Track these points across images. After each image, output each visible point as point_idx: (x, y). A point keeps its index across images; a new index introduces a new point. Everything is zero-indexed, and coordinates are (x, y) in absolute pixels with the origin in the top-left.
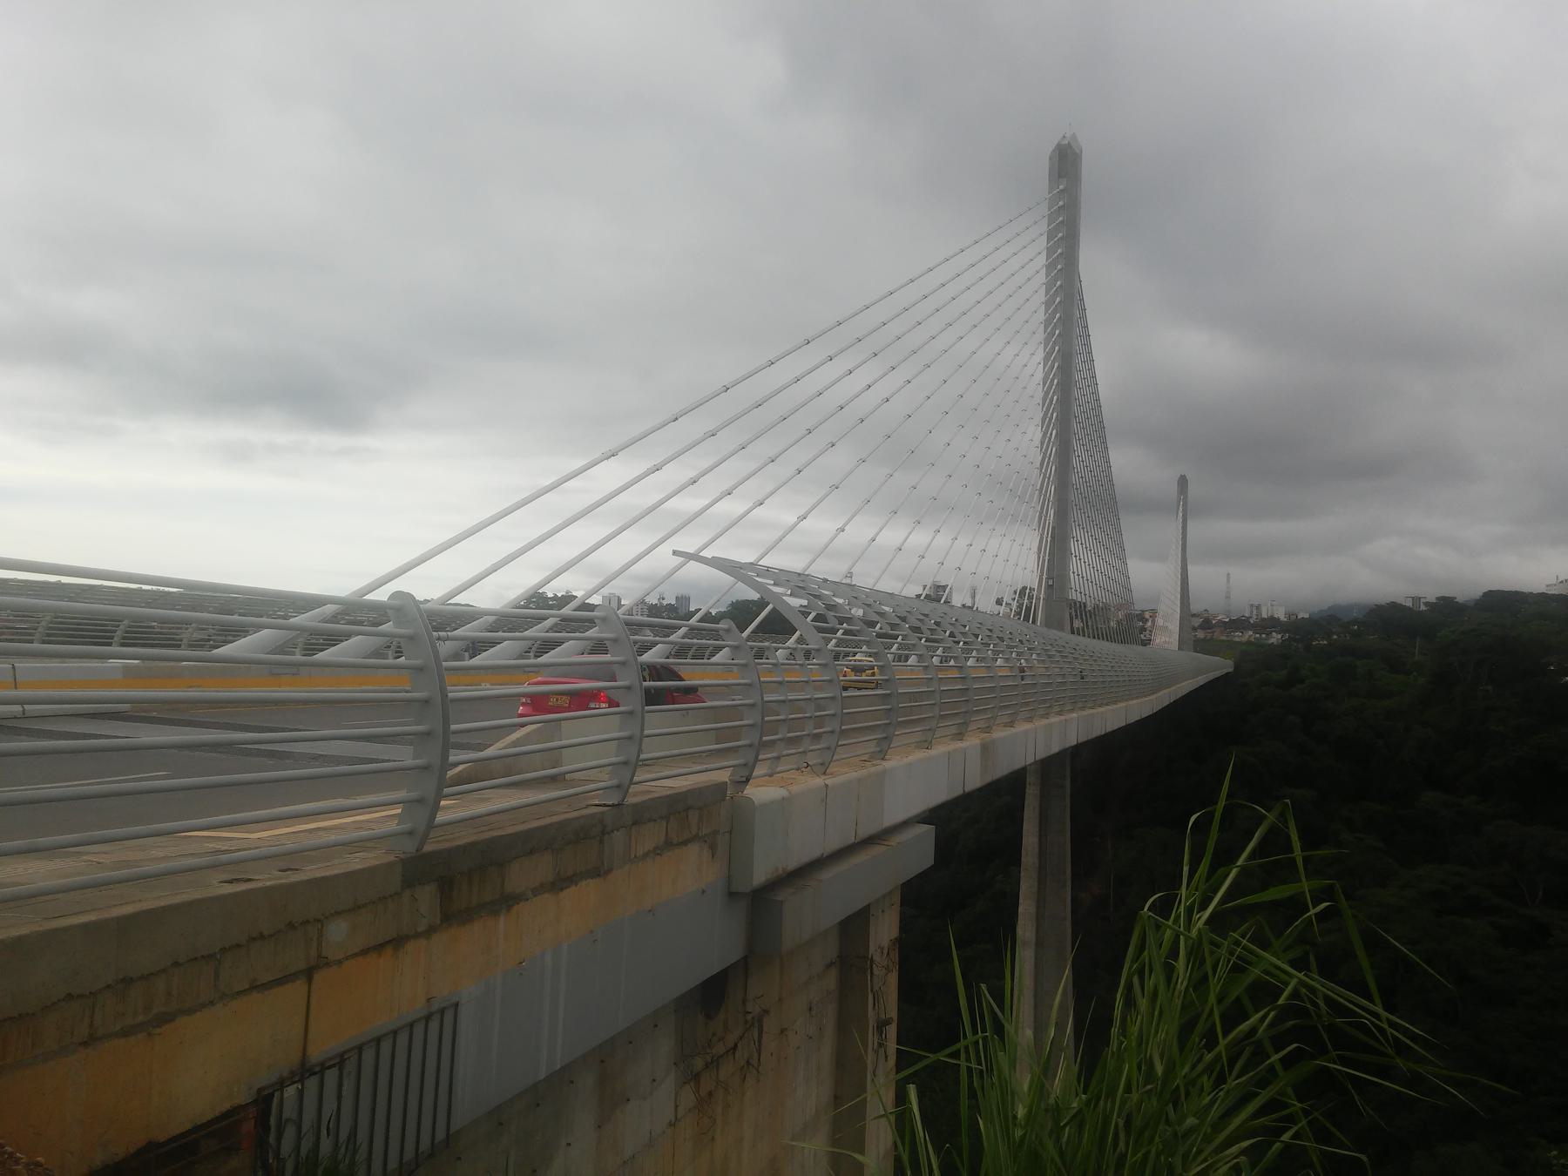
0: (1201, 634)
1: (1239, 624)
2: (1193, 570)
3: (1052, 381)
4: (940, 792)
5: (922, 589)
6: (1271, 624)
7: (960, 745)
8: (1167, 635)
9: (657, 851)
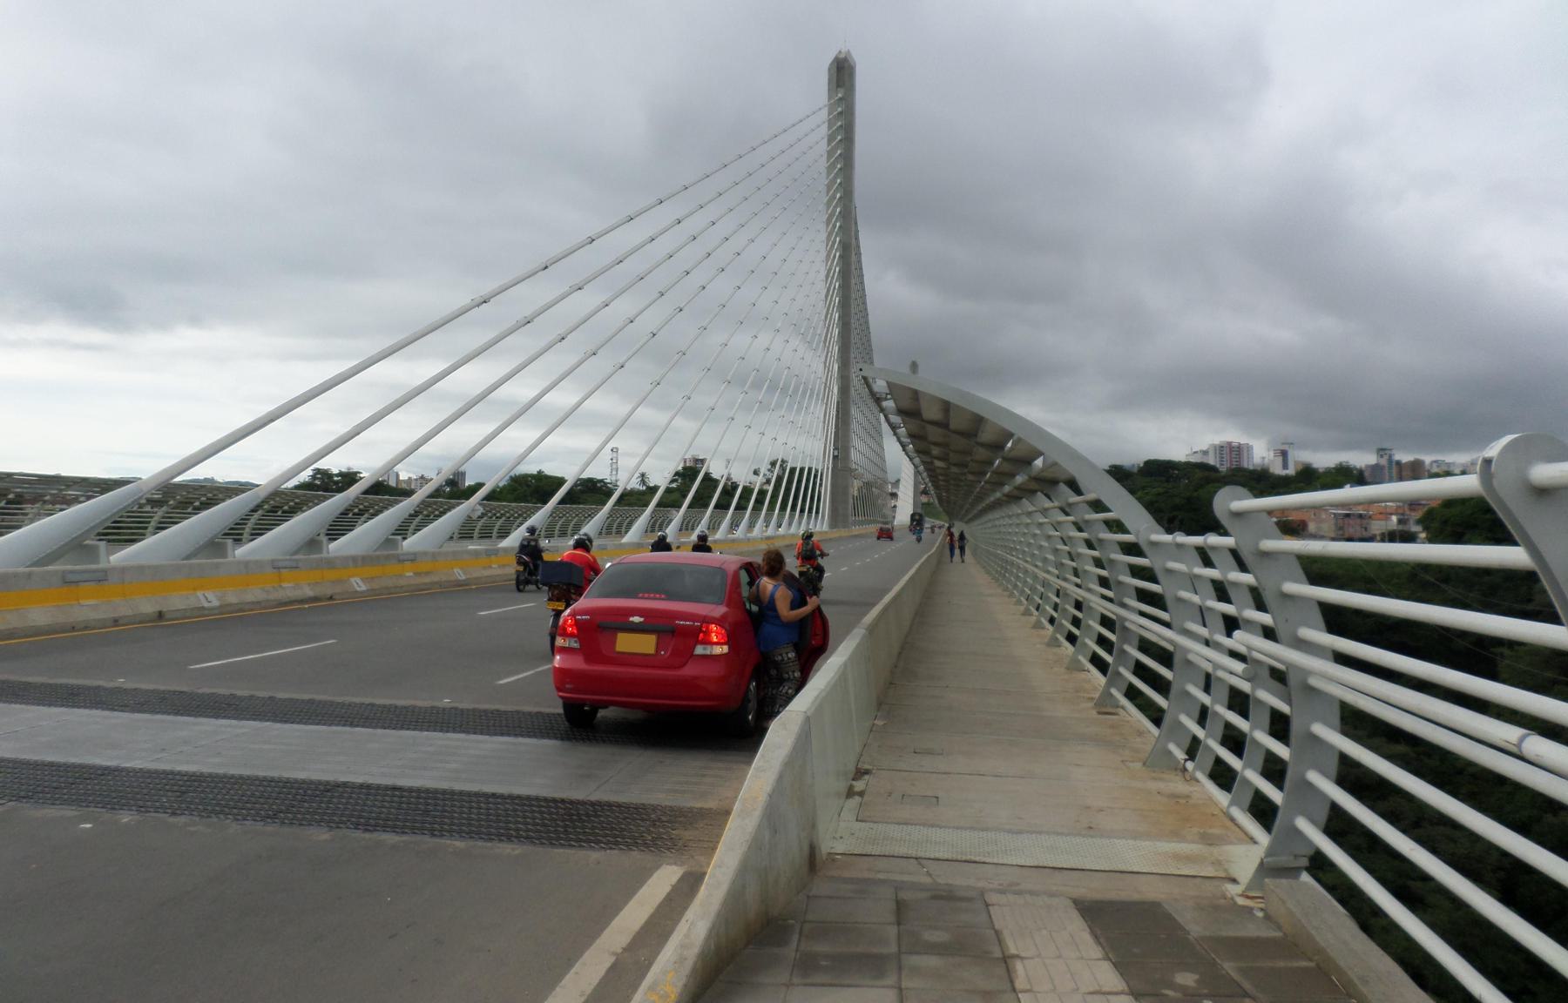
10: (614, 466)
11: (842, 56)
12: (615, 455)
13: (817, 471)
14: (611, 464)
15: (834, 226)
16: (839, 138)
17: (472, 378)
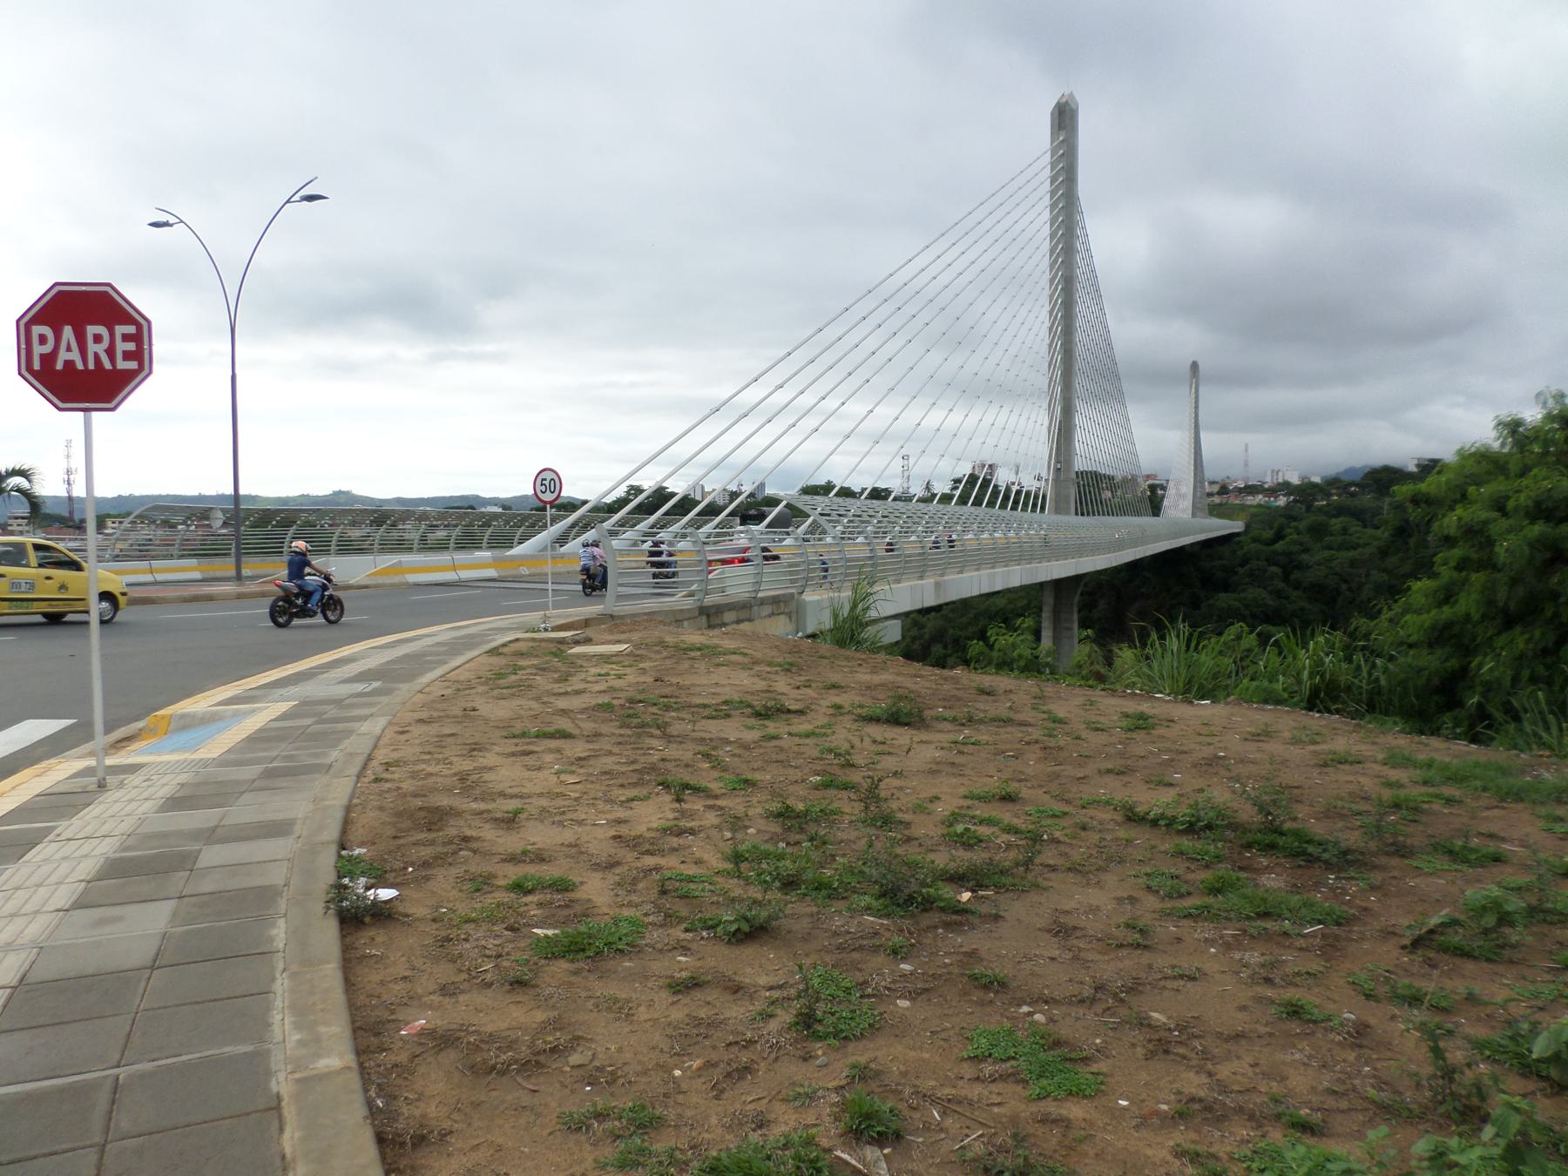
0: (1217, 500)
1: (1251, 490)
2: (1204, 436)
3: (1057, 300)
4: (907, 606)
5: (950, 485)
6: (1286, 487)
7: (920, 582)
8: (1179, 504)
9: (770, 616)
10: (906, 474)
11: (1064, 100)
12: (906, 462)
13: (674, 574)
14: (903, 472)
15: (1056, 289)
16: (1061, 179)
17: (807, 400)
